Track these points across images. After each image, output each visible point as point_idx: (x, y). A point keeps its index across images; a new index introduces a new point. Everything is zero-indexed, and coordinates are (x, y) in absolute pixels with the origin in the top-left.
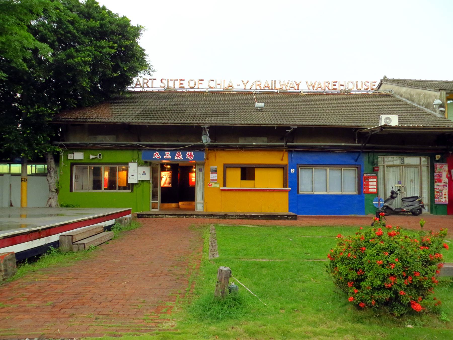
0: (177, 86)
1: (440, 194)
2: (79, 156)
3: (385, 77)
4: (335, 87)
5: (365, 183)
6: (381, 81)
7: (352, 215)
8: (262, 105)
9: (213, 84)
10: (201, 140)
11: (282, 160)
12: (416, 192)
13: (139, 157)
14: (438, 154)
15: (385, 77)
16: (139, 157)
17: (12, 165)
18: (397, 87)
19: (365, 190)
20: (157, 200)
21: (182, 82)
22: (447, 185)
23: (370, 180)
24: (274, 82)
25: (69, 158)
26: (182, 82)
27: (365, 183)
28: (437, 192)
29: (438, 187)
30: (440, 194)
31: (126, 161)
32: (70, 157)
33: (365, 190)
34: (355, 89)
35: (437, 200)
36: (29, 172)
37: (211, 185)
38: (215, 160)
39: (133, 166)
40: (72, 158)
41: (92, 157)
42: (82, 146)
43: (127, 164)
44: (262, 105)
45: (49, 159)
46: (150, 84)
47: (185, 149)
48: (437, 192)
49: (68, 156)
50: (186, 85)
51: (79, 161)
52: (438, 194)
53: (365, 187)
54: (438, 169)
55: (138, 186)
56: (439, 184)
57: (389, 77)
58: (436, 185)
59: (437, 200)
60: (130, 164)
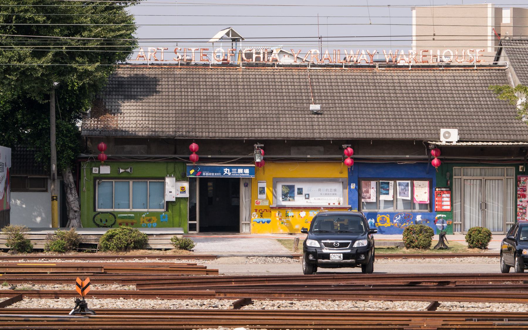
1: (524, 211)
5: (437, 199)
10: (340, 224)
12: (499, 211)
13: (175, 171)
14: (521, 165)
16: (175, 171)
18: (160, 302)
19: (437, 207)
20: (195, 220)
23: (444, 195)
25: (94, 172)
27: (437, 199)
28: (520, 209)
29: (521, 204)
30: (524, 211)
31: (163, 176)
32: (95, 170)
33: (437, 207)
35: (520, 218)
36: (448, 208)
37: (259, 203)
38: (264, 173)
39: (169, 181)
40: (97, 172)
41: (121, 171)
42: (113, 159)
43: (164, 179)
45: (67, 173)
47: (244, 168)
48: (520, 209)
49: (92, 169)
51: (106, 176)
52: (521, 211)
53: (437, 203)
54: (521, 182)
55: (173, 204)
56: (523, 199)
58: (518, 200)
59: (520, 218)
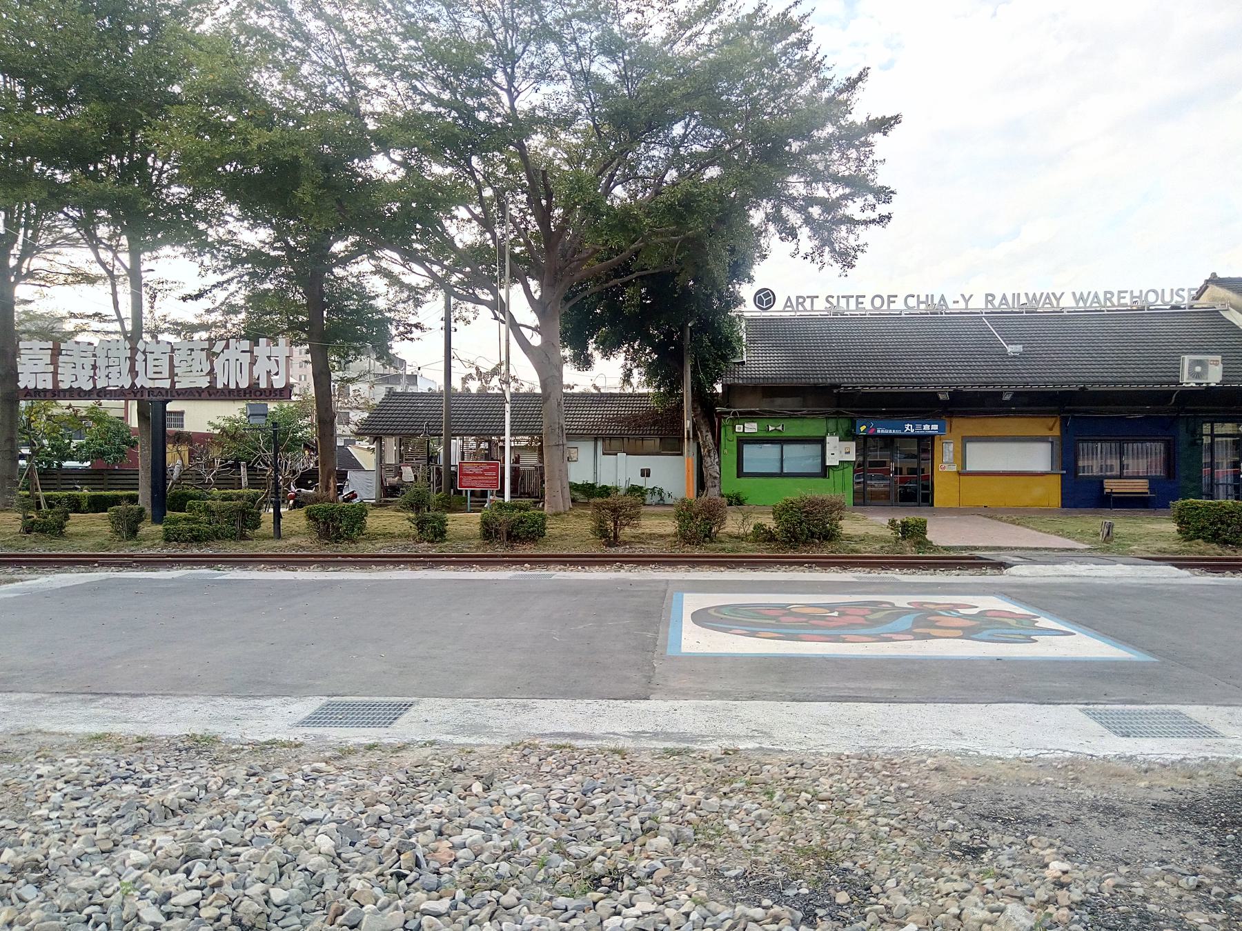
0: (853, 305)
2: (751, 428)
3: (1214, 275)
4: (1122, 301)
6: (1207, 281)
7: (12, 595)
8: (1019, 348)
9: (912, 302)
11: (1051, 429)
15: (1214, 275)
17: (785, 447)
21: (860, 300)
22: (629, 390)
24: (1017, 296)
26: (860, 300)
32: (739, 429)
34: (1159, 302)
44: (1019, 348)
46: (808, 304)
50: (867, 305)
57: (1221, 275)
60: (828, 439)
